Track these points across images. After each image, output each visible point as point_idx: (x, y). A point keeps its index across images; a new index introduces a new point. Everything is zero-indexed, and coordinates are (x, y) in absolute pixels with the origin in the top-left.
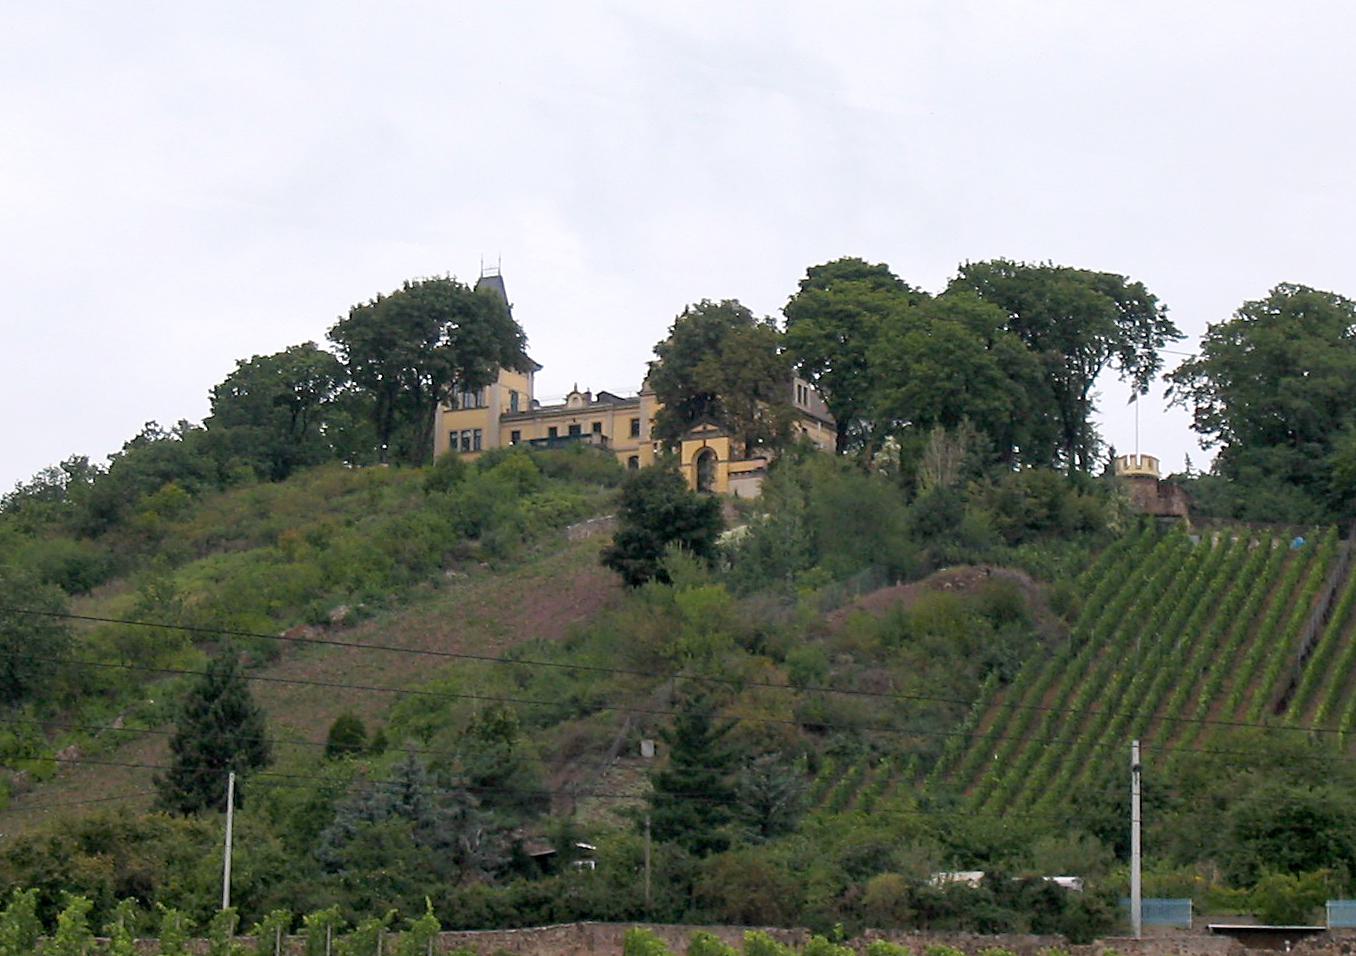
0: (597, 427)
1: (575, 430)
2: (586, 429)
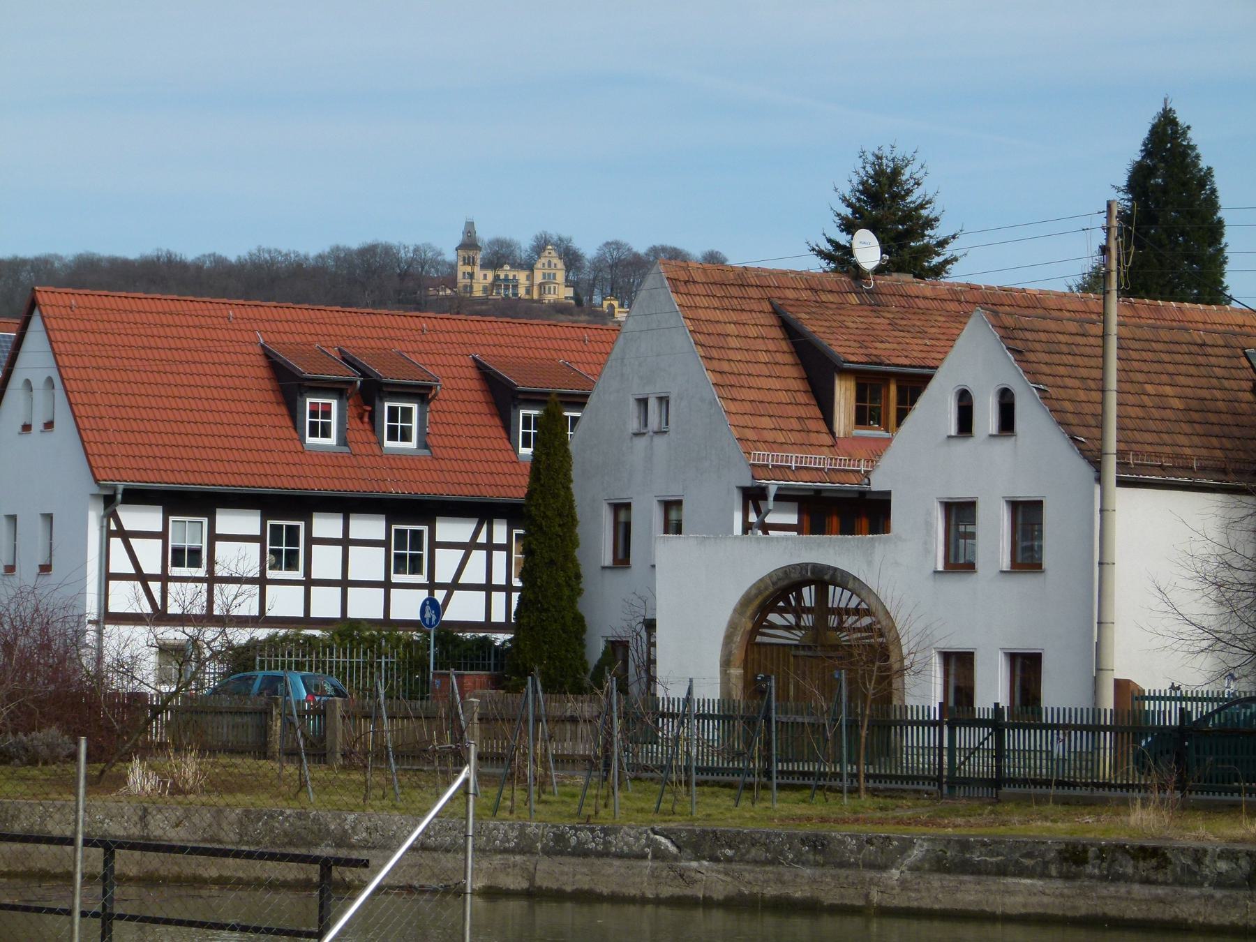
0: (514, 276)
1: (506, 276)
2: (511, 277)
